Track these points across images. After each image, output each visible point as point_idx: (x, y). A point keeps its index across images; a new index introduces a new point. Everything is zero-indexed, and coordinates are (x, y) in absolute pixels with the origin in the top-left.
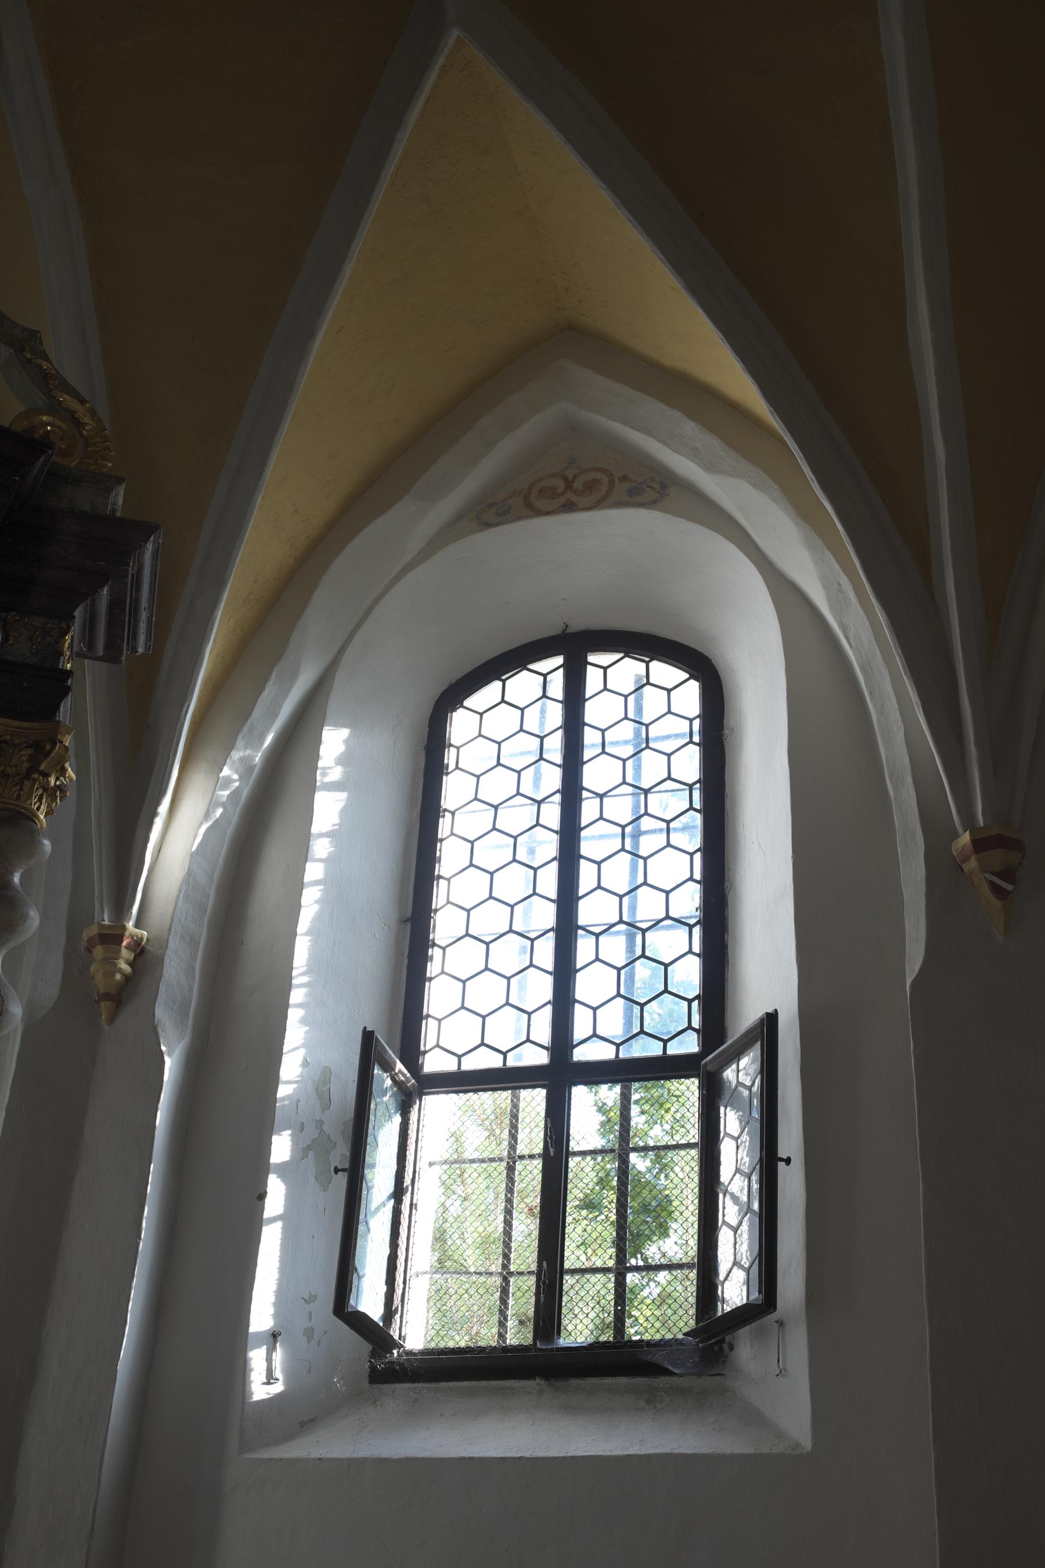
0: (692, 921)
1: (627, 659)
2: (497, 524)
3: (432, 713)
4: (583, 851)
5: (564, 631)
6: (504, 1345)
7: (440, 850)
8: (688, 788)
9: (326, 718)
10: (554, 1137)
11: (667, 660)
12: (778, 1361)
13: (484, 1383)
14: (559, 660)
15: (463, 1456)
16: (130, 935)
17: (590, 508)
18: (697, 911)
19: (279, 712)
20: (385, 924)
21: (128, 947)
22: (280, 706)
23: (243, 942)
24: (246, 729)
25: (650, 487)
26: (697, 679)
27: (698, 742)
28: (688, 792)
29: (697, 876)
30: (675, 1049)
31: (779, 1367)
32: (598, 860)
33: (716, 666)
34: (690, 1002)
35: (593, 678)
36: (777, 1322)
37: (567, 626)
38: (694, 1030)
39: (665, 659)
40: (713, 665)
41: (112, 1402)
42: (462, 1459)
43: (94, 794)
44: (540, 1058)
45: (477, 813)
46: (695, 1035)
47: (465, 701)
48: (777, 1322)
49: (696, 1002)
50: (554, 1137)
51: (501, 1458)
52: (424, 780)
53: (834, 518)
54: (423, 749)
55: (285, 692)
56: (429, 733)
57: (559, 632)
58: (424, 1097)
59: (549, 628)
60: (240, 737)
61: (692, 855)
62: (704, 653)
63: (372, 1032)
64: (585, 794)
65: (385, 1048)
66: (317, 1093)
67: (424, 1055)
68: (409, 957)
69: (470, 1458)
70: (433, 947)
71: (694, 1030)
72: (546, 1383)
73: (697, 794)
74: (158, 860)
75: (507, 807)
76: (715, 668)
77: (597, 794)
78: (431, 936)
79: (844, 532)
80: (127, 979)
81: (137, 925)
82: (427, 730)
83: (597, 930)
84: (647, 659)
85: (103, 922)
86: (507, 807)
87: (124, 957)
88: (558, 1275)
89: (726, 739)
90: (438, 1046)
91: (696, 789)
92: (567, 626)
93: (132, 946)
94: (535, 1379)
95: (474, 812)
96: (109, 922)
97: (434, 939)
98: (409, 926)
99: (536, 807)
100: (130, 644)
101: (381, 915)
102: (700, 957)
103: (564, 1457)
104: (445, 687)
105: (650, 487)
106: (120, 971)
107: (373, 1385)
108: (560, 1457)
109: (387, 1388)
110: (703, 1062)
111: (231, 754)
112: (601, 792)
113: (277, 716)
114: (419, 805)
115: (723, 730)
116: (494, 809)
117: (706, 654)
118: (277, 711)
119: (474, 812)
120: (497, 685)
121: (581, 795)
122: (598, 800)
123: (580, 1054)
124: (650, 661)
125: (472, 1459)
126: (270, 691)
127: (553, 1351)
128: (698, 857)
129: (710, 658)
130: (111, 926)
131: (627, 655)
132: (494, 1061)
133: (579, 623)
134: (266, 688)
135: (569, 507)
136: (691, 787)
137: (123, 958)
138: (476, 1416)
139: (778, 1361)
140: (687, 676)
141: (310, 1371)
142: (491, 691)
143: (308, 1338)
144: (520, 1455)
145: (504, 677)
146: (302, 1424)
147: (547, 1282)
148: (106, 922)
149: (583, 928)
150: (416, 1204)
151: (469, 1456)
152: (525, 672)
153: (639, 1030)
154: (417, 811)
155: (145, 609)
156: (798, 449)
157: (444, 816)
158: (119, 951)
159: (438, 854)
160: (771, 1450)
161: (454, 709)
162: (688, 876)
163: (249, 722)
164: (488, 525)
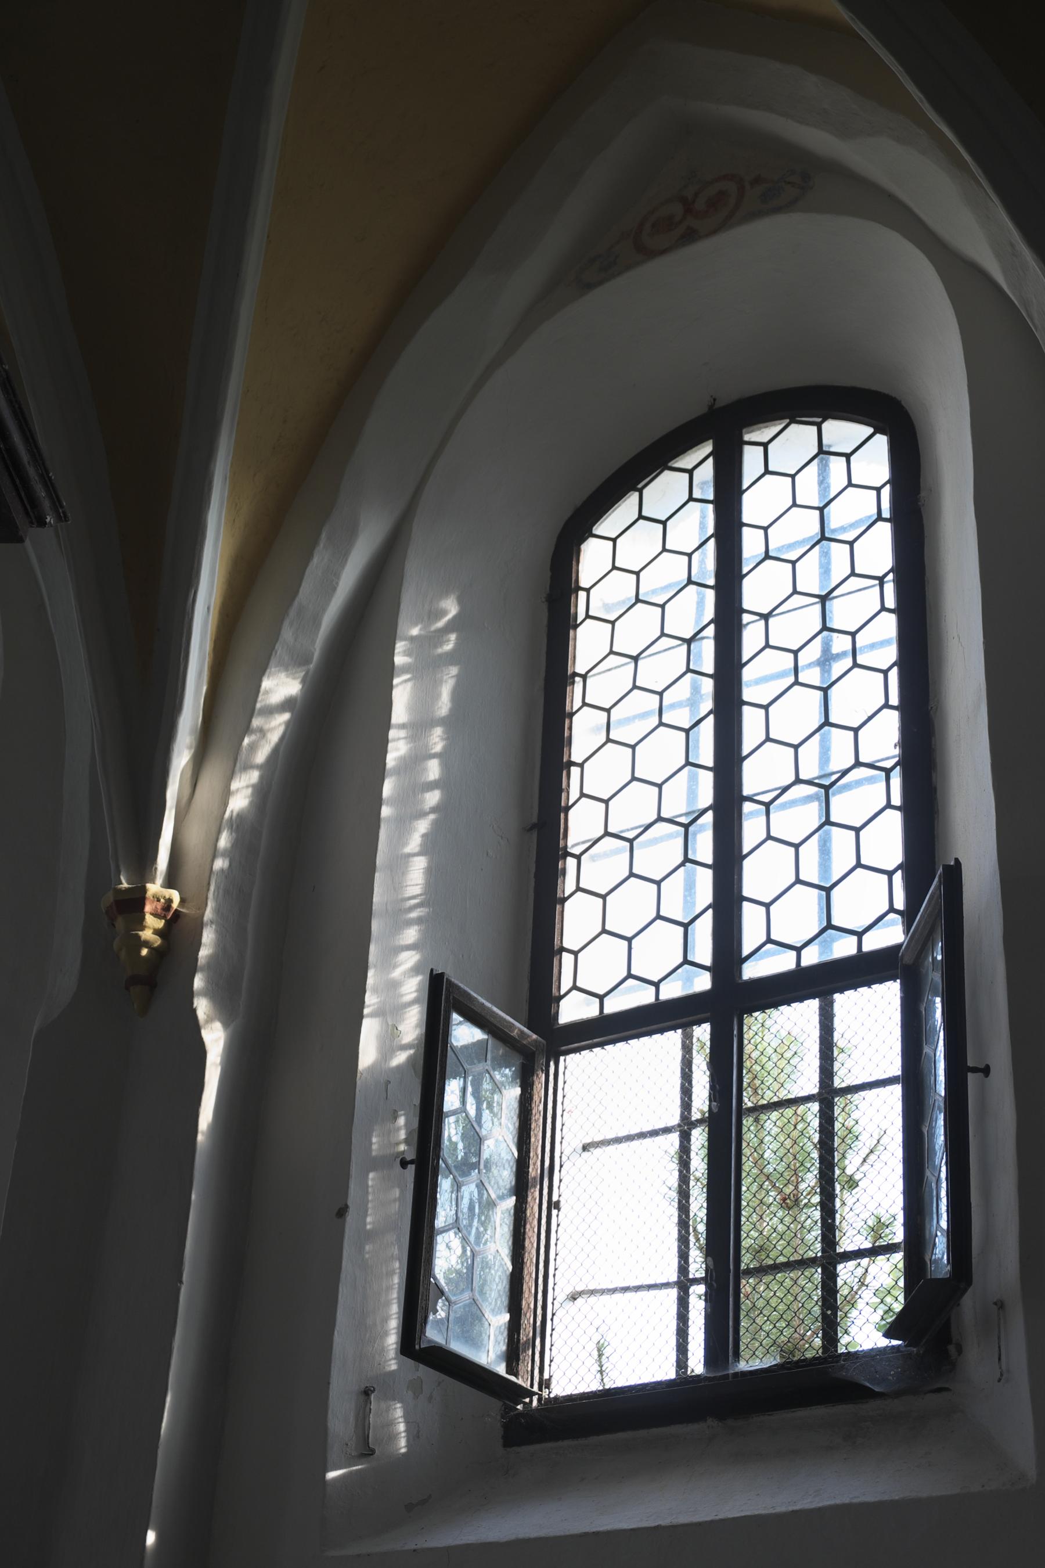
0: (888, 764)
1: (794, 427)
2: (601, 283)
3: (554, 551)
4: (746, 697)
5: (711, 407)
6: (685, 1376)
7: (570, 728)
8: (877, 582)
9: (404, 581)
10: (717, 1086)
11: (845, 414)
12: (1000, 1359)
13: (642, 1433)
14: (707, 448)
15: (587, 1531)
16: (153, 897)
17: (715, 232)
18: (895, 748)
19: (337, 583)
20: (502, 837)
21: (155, 915)
22: (337, 576)
23: (314, 887)
24: (292, 612)
25: (789, 183)
26: (883, 433)
27: (888, 517)
28: (878, 588)
29: (894, 700)
30: (873, 942)
31: (1000, 1368)
32: (765, 703)
33: (907, 408)
34: (890, 874)
35: (752, 460)
36: (995, 1304)
37: (715, 400)
38: (897, 912)
39: (855, 416)
40: (903, 407)
41: (152, 1495)
42: (585, 1535)
43: (95, 724)
44: (703, 982)
45: (613, 671)
46: (897, 918)
47: (594, 528)
48: (995, 1304)
49: (899, 873)
50: (717, 1086)
51: (632, 1530)
52: (548, 641)
53: (957, 146)
54: (544, 600)
55: (342, 556)
56: (552, 578)
57: (704, 410)
58: (562, 1058)
59: (694, 409)
60: (286, 624)
61: (885, 673)
62: (890, 394)
63: (442, 975)
64: (746, 618)
65: (469, 994)
66: (414, 1069)
67: (558, 1003)
68: (536, 876)
69: (594, 1532)
70: (565, 858)
71: (897, 912)
72: (720, 1424)
73: (890, 588)
74: (193, 801)
75: (650, 655)
76: (906, 411)
77: (762, 616)
78: (562, 843)
79: (973, 163)
80: (158, 953)
81: (170, 882)
82: (549, 574)
83: (766, 798)
84: (820, 420)
85: (121, 886)
86: (650, 655)
87: (152, 927)
88: (731, 1274)
89: (923, 505)
90: (575, 987)
91: (889, 581)
92: (715, 400)
93: (159, 911)
94: (706, 1421)
95: (609, 670)
96: (128, 884)
97: (566, 846)
98: (535, 835)
99: (685, 646)
100: (31, 514)
101: (495, 826)
102: (901, 812)
103: (712, 1521)
104: (568, 514)
105: (789, 183)
106: (146, 944)
107: (508, 1449)
108: (706, 1522)
109: (526, 1450)
110: (900, 954)
111: (276, 648)
112: (765, 611)
113: (334, 589)
114: (543, 674)
115: (919, 493)
116: (633, 661)
117: (894, 396)
118: (334, 583)
119: (609, 670)
120: (633, 498)
121: (740, 620)
122: (763, 622)
123: (751, 971)
124: (823, 422)
125: (596, 1534)
126: (319, 560)
127: (728, 1378)
128: (894, 675)
129: (899, 398)
130: (129, 888)
131: (793, 421)
132: (645, 997)
133: (730, 392)
134: (315, 555)
135: (690, 236)
136: (881, 580)
137: (149, 928)
138: (623, 1477)
139: (1000, 1359)
140: (871, 430)
141: (418, 1437)
142: (625, 510)
143: (415, 1394)
144: (657, 1524)
145: (640, 486)
146: (409, 1507)
147: (715, 1285)
148: (125, 885)
149: (749, 799)
150: (558, 1202)
151: (594, 1530)
152: (667, 473)
153: (825, 924)
154: (540, 683)
155: (29, 462)
156: (895, 62)
157: (573, 683)
158: (143, 918)
159: (566, 734)
160: (983, 1486)
161: (583, 540)
162: (882, 702)
163: (296, 603)
164: (589, 287)
